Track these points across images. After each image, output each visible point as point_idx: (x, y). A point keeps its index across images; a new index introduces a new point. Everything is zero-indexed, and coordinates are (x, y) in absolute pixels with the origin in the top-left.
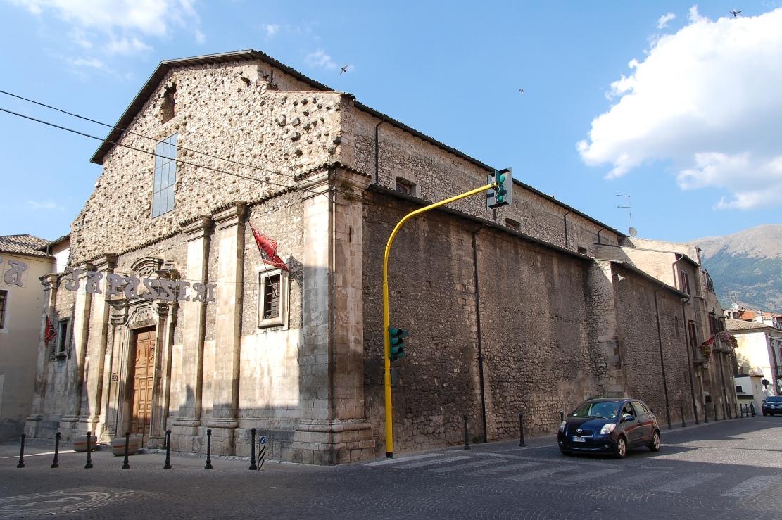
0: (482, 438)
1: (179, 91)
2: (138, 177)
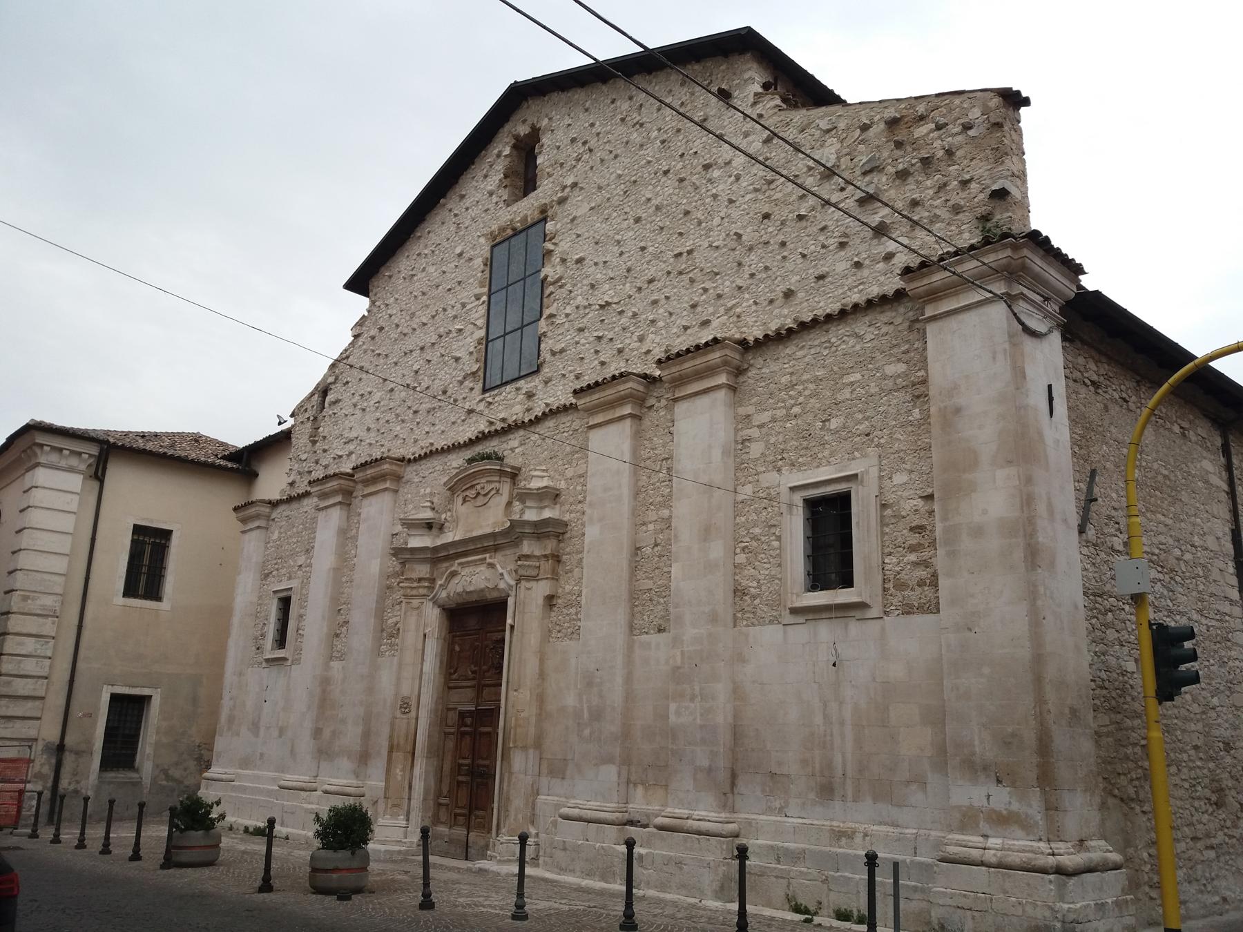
0: (866, 835)
1: (546, 140)
2: (451, 313)
